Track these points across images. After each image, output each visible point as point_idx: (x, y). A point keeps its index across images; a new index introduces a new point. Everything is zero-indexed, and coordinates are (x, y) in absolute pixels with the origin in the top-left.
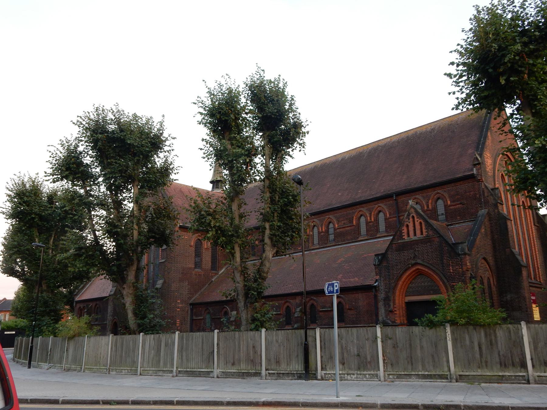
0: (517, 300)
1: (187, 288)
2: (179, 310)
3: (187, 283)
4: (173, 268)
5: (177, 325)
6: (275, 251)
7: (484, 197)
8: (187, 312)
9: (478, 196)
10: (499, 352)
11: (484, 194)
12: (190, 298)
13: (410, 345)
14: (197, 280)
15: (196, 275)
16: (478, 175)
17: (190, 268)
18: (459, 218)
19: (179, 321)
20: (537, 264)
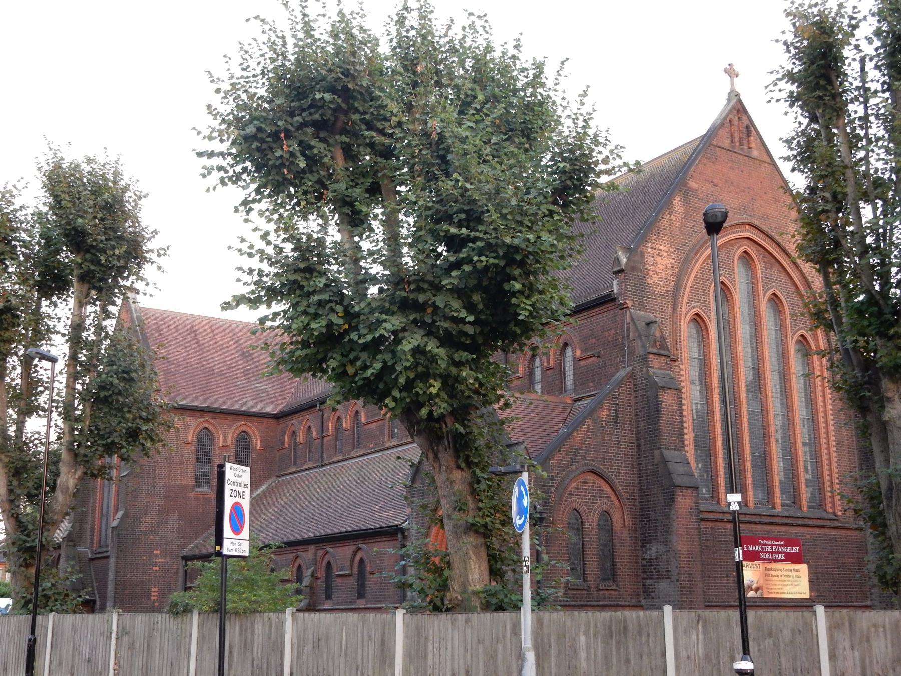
0: (665, 557)
1: (176, 526)
2: (157, 569)
3: (176, 517)
4: (145, 487)
5: (152, 598)
6: (79, 473)
7: (629, 342)
8: (176, 573)
9: (620, 338)
10: (253, 661)
11: (628, 336)
12: (183, 546)
13: (148, 646)
14: (201, 510)
15: (197, 499)
16: (620, 294)
17: (185, 487)
18: (591, 384)
19: (156, 590)
20: (831, 475)
